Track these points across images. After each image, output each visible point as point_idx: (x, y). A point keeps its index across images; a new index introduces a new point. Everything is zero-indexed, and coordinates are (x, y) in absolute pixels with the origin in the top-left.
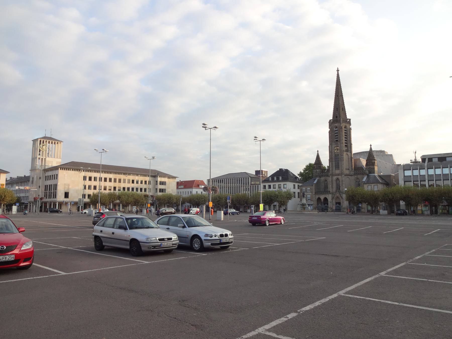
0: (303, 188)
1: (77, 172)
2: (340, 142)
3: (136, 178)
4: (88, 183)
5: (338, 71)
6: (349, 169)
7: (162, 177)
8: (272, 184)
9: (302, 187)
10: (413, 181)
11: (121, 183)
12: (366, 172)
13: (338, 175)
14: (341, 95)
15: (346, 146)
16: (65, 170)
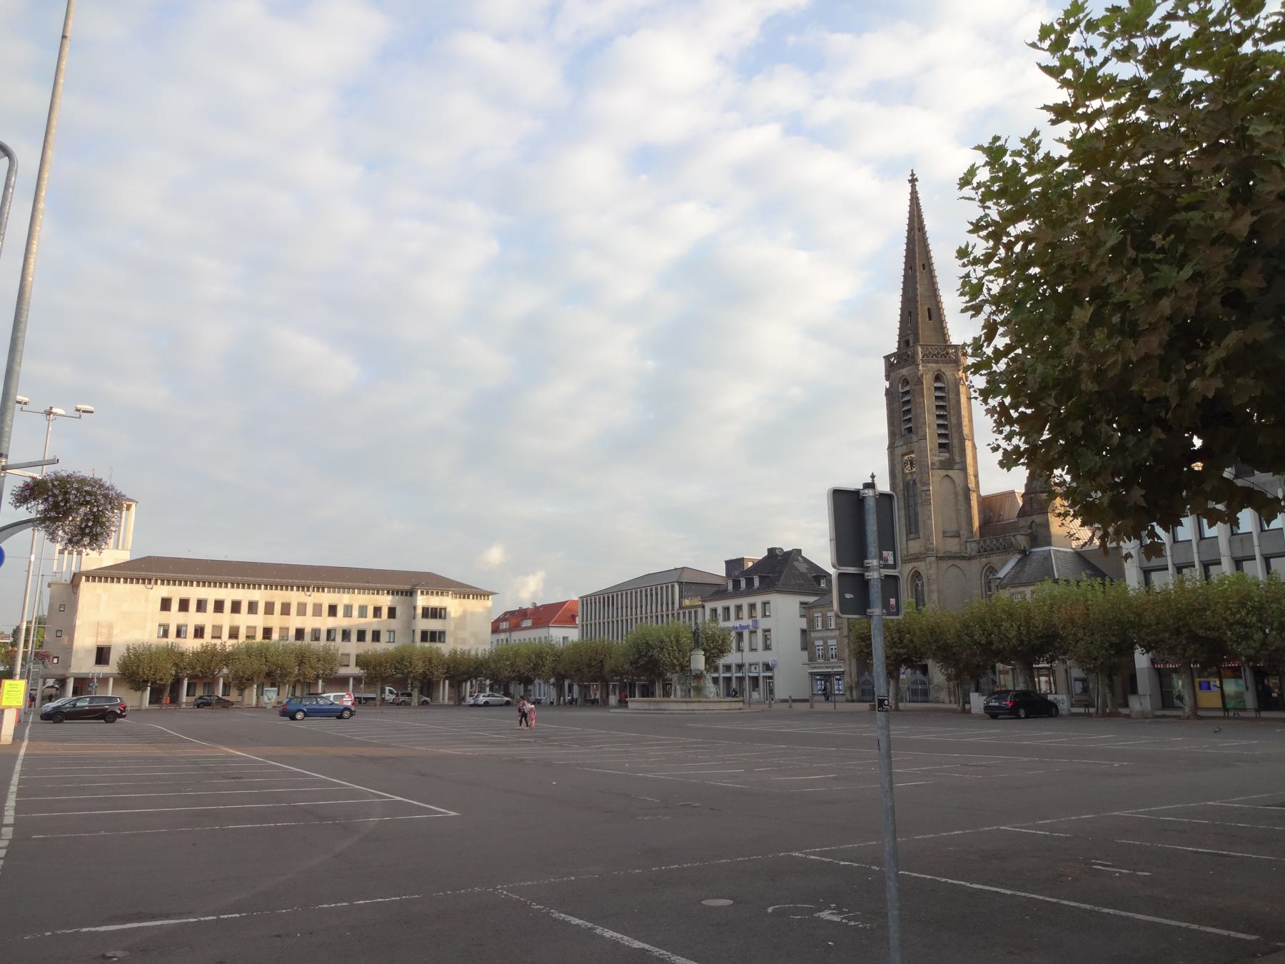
1: (141, 587)
2: (917, 434)
3: (342, 599)
4: (174, 617)
5: (913, 181)
6: (958, 532)
7: (432, 593)
8: (732, 603)
10: (1201, 562)
11: (289, 614)
12: (1016, 540)
14: (924, 265)
15: (941, 446)
16: (249, 588)
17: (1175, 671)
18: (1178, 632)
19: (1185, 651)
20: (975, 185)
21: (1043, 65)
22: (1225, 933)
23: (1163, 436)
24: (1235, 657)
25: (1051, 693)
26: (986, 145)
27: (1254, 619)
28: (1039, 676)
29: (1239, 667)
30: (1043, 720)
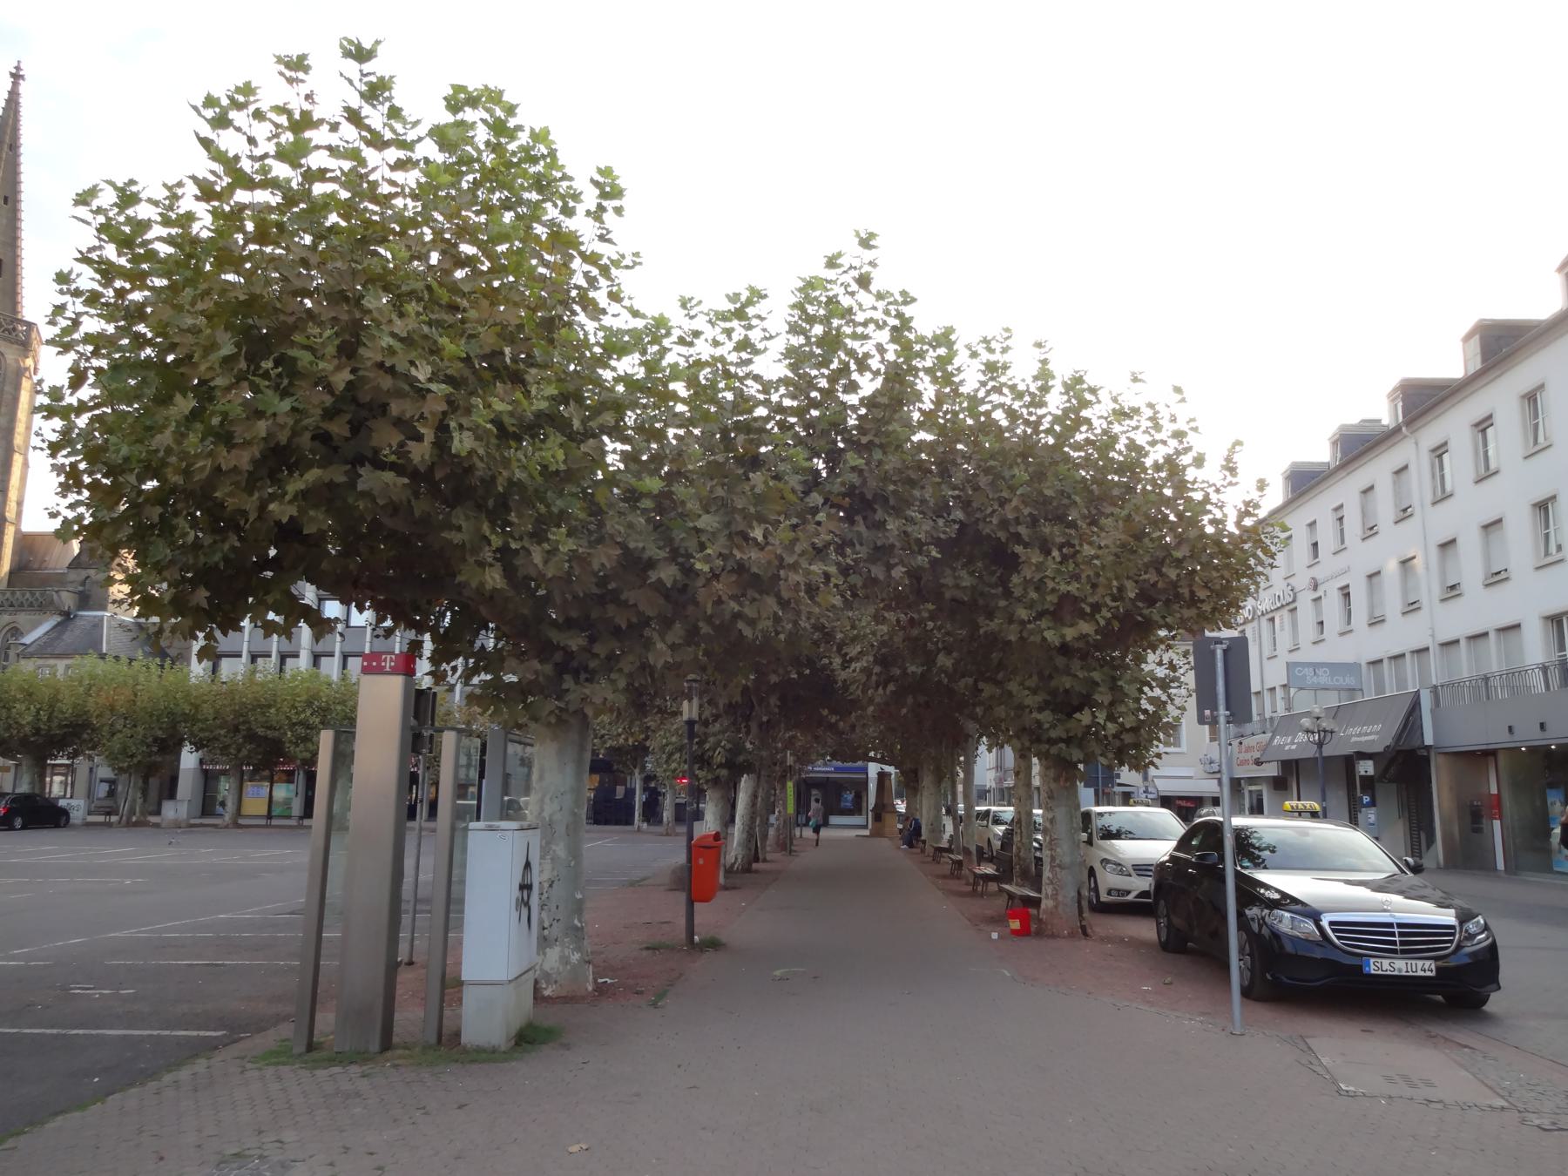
5: (17, 77)
10: (279, 652)
12: (59, 597)
17: (224, 773)
18: (236, 730)
19: (239, 751)
20: (94, 208)
21: (202, 135)
22: (195, 1033)
23: (237, 544)
24: (290, 759)
25: (64, 797)
26: (120, 184)
27: (318, 720)
28: (53, 774)
29: (293, 771)
30: (45, 832)
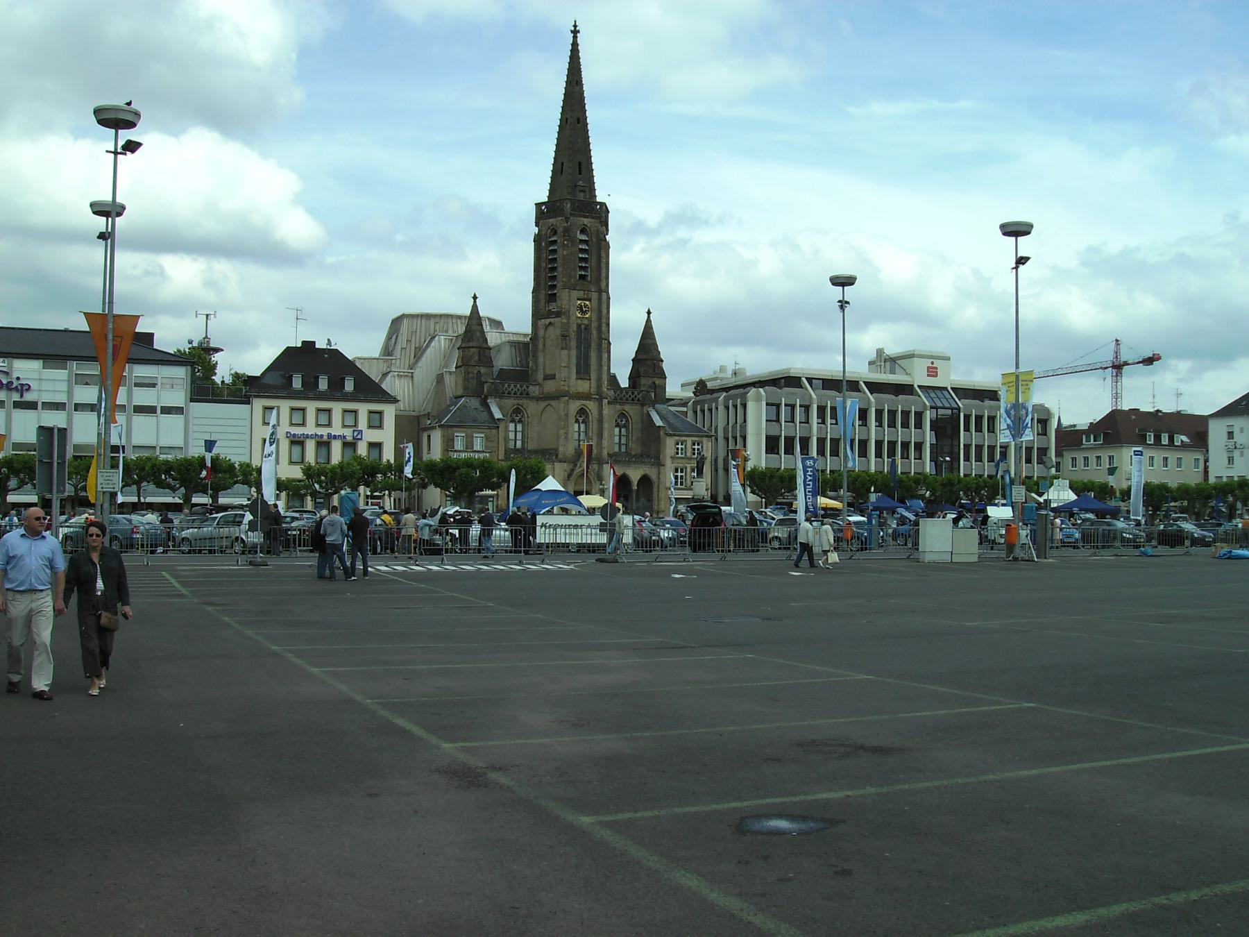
0: (457, 432)
9: (454, 429)
13: (587, 397)
